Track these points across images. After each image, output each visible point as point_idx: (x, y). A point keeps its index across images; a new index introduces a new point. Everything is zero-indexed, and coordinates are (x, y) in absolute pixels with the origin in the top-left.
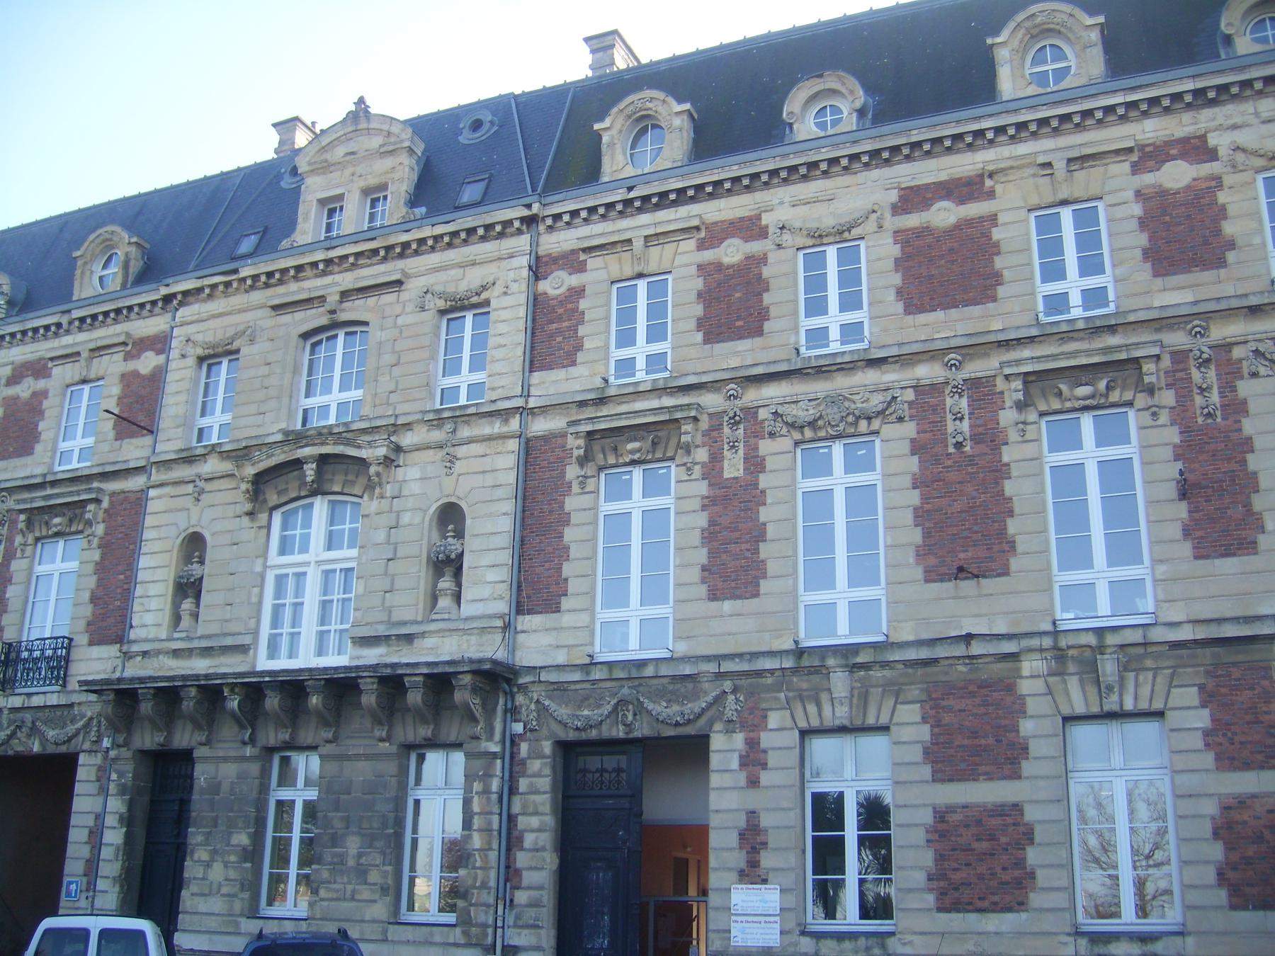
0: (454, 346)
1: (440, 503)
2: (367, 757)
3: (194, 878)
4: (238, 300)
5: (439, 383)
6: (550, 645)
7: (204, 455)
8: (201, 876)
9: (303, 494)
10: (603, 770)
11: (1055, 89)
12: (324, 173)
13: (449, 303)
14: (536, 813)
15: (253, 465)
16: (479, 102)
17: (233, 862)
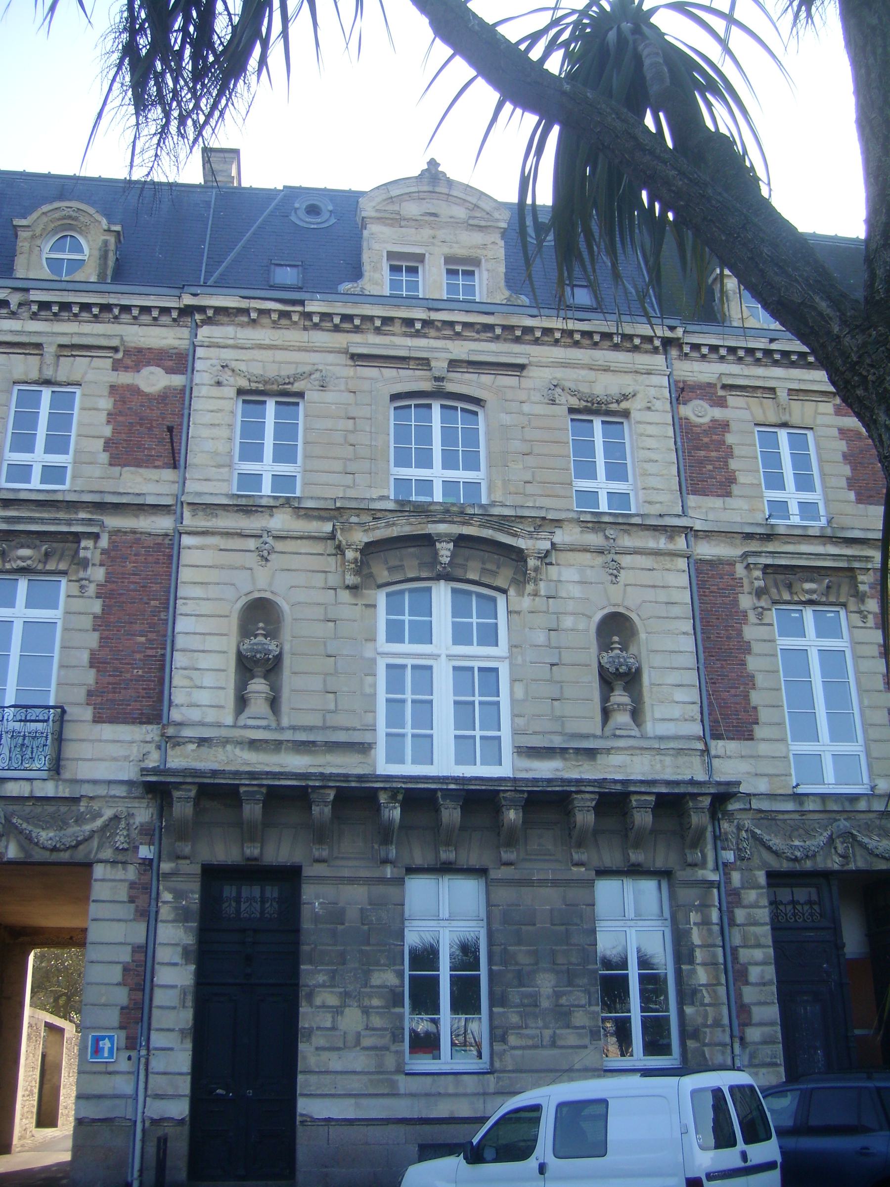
0: (253, 430)
1: (606, 611)
2: (555, 883)
3: (319, 1028)
4: (294, 336)
5: (298, 469)
6: (748, 773)
7: (271, 507)
8: (328, 1024)
9: (424, 575)
10: (793, 903)
12: (392, 226)
13: (585, 404)
14: (758, 946)
15: (365, 531)
16: (325, 190)
17: (377, 1007)
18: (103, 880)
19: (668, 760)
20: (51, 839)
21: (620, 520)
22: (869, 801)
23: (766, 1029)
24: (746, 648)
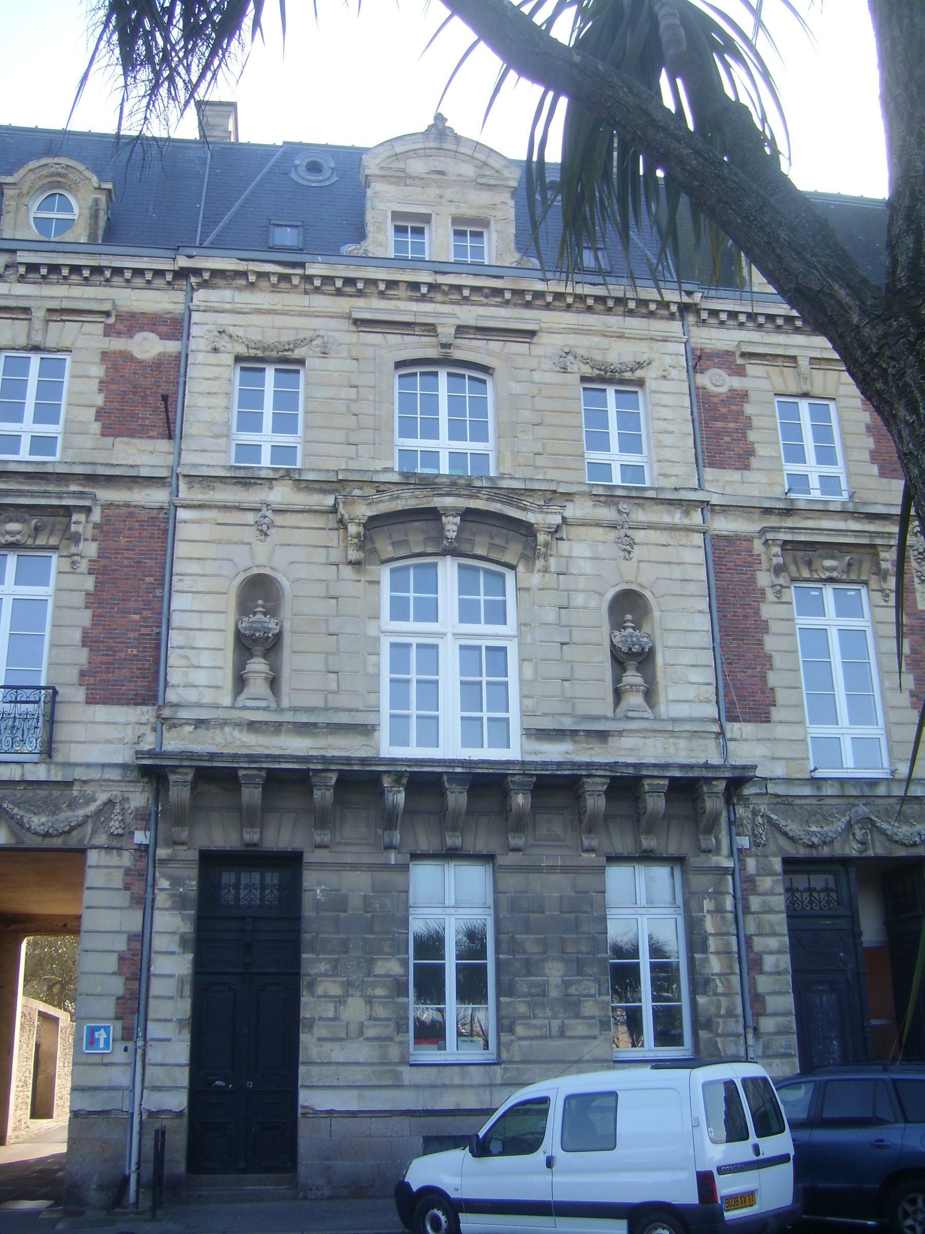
1: (618, 588)
3: (320, 1018)
6: (765, 757)
8: (331, 1014)
10: (810, 890)
11: (56, 239)
12: (397, 184)
13: (598, 372)
14: (773, 934)
17: (381, 997)
18: (97, 867)
19: (682, 743)
20: (43, 824)
21: (634, 494)
22: (889, 787)
23: (780, 1020)
24: (764, 627)
